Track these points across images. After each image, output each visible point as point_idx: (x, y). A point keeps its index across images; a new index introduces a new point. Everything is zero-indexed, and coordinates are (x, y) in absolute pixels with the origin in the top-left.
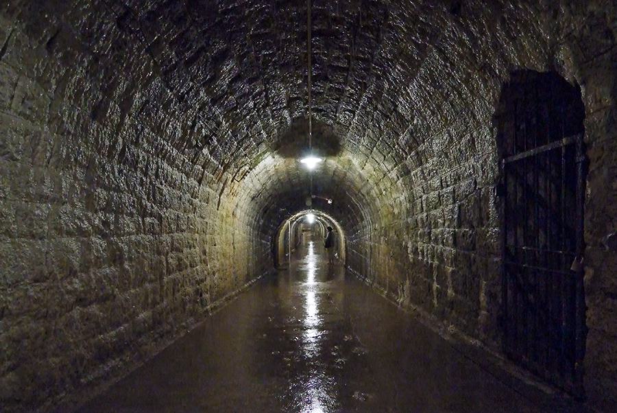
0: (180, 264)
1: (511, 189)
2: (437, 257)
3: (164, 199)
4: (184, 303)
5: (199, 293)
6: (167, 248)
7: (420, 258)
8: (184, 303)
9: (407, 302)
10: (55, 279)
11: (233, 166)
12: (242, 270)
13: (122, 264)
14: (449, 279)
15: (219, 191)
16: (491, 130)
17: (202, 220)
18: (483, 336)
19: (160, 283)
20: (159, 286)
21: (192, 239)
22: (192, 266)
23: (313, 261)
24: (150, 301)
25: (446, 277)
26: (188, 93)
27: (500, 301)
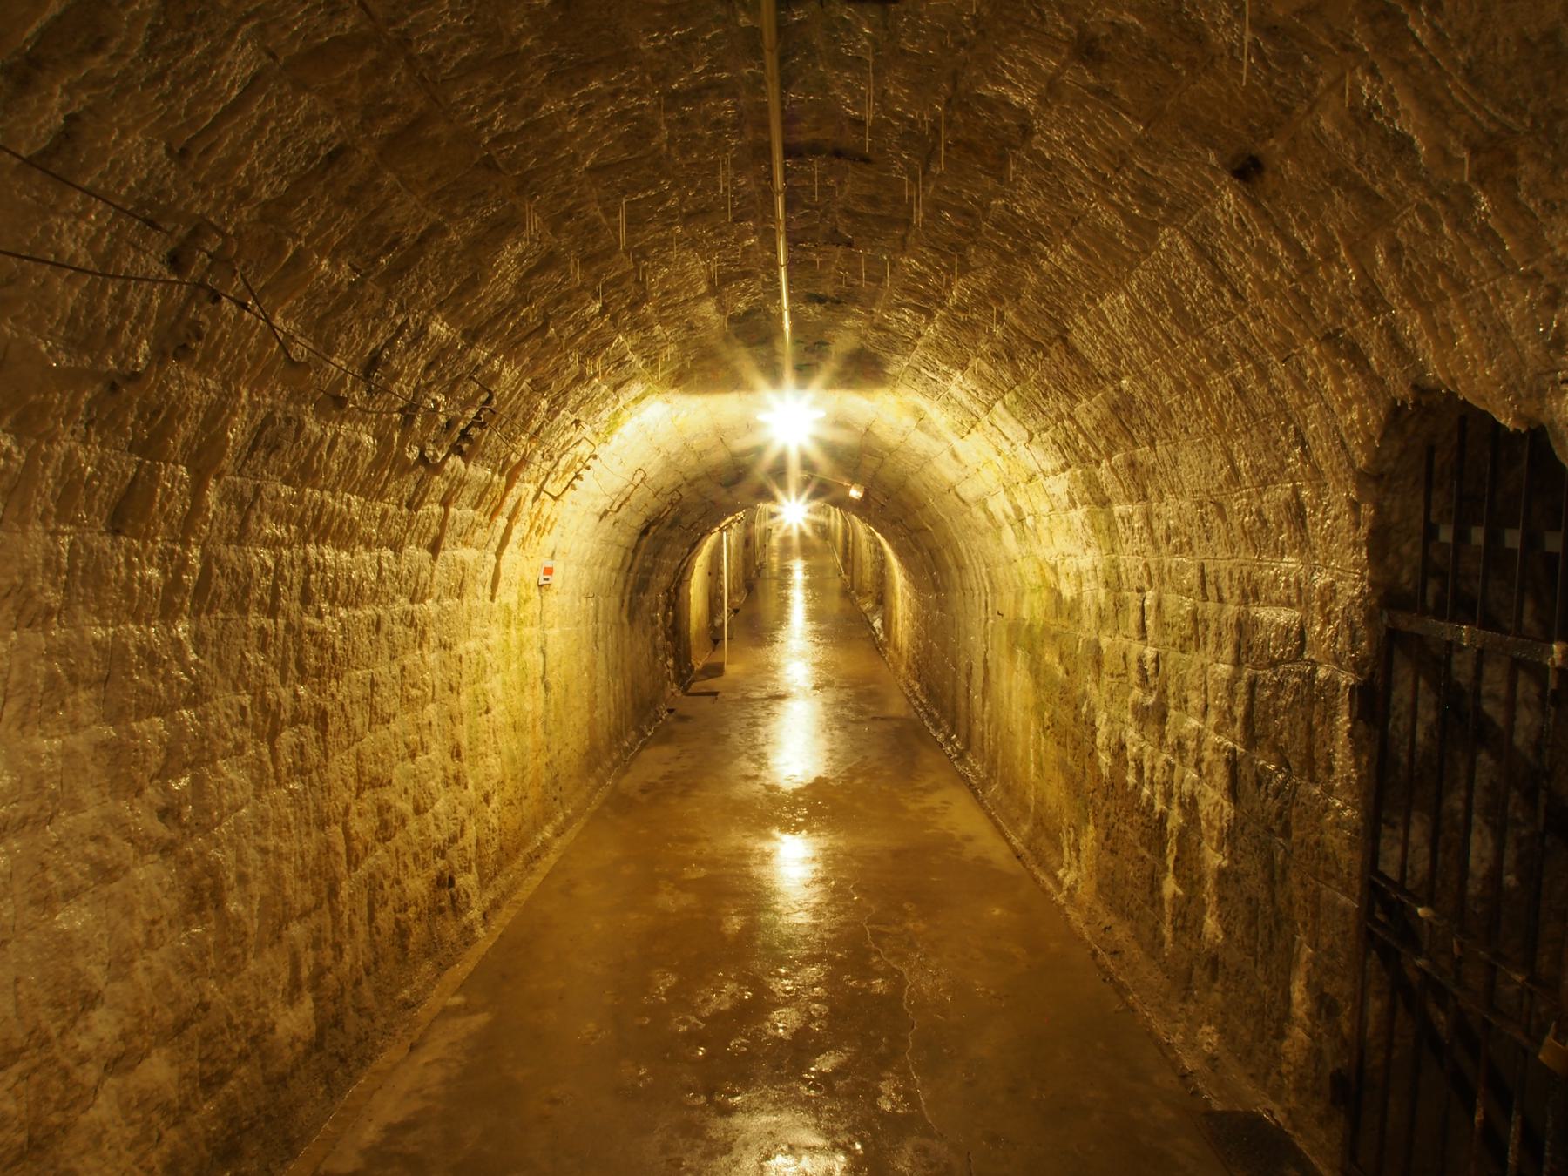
0: (384, 825)
1: (1401, 693)
2: (1182, 805)
3: (328, 656)
4: (402, 932)
5: (445, 882)
6: (346, 795)
7: (1131, 779)
8: (402, 932)
9: (1085, 892)
10: (45, 1042)
11: (538, 458)
12: (572, 739)
13: (219, 904)
14: (1209, 885)
15: (494, 546)
16: (1355, 506)
17: (445, 654)
18: (1293, 1101)
19: (332, 909)
20: (328, 919)
21: (419, 728)
22: (418, 811)
23: (802, 655)
24: (305, 973)
25: (1201, 879)
26: (390, 343)
27: (1346, 1027)
